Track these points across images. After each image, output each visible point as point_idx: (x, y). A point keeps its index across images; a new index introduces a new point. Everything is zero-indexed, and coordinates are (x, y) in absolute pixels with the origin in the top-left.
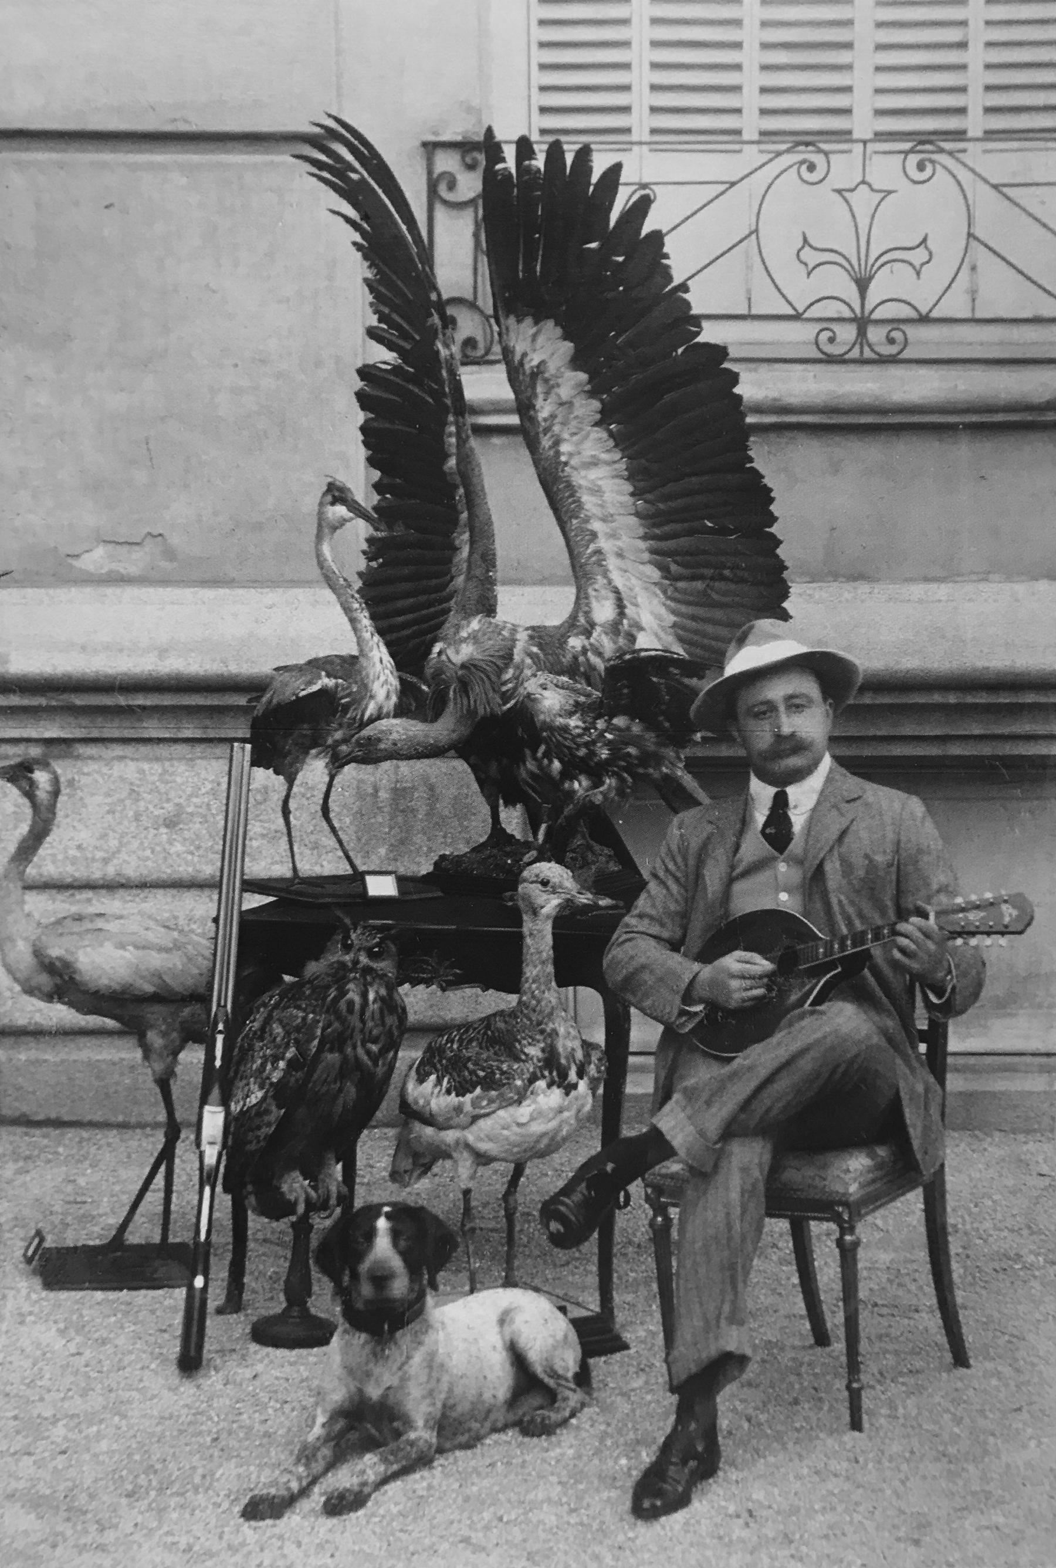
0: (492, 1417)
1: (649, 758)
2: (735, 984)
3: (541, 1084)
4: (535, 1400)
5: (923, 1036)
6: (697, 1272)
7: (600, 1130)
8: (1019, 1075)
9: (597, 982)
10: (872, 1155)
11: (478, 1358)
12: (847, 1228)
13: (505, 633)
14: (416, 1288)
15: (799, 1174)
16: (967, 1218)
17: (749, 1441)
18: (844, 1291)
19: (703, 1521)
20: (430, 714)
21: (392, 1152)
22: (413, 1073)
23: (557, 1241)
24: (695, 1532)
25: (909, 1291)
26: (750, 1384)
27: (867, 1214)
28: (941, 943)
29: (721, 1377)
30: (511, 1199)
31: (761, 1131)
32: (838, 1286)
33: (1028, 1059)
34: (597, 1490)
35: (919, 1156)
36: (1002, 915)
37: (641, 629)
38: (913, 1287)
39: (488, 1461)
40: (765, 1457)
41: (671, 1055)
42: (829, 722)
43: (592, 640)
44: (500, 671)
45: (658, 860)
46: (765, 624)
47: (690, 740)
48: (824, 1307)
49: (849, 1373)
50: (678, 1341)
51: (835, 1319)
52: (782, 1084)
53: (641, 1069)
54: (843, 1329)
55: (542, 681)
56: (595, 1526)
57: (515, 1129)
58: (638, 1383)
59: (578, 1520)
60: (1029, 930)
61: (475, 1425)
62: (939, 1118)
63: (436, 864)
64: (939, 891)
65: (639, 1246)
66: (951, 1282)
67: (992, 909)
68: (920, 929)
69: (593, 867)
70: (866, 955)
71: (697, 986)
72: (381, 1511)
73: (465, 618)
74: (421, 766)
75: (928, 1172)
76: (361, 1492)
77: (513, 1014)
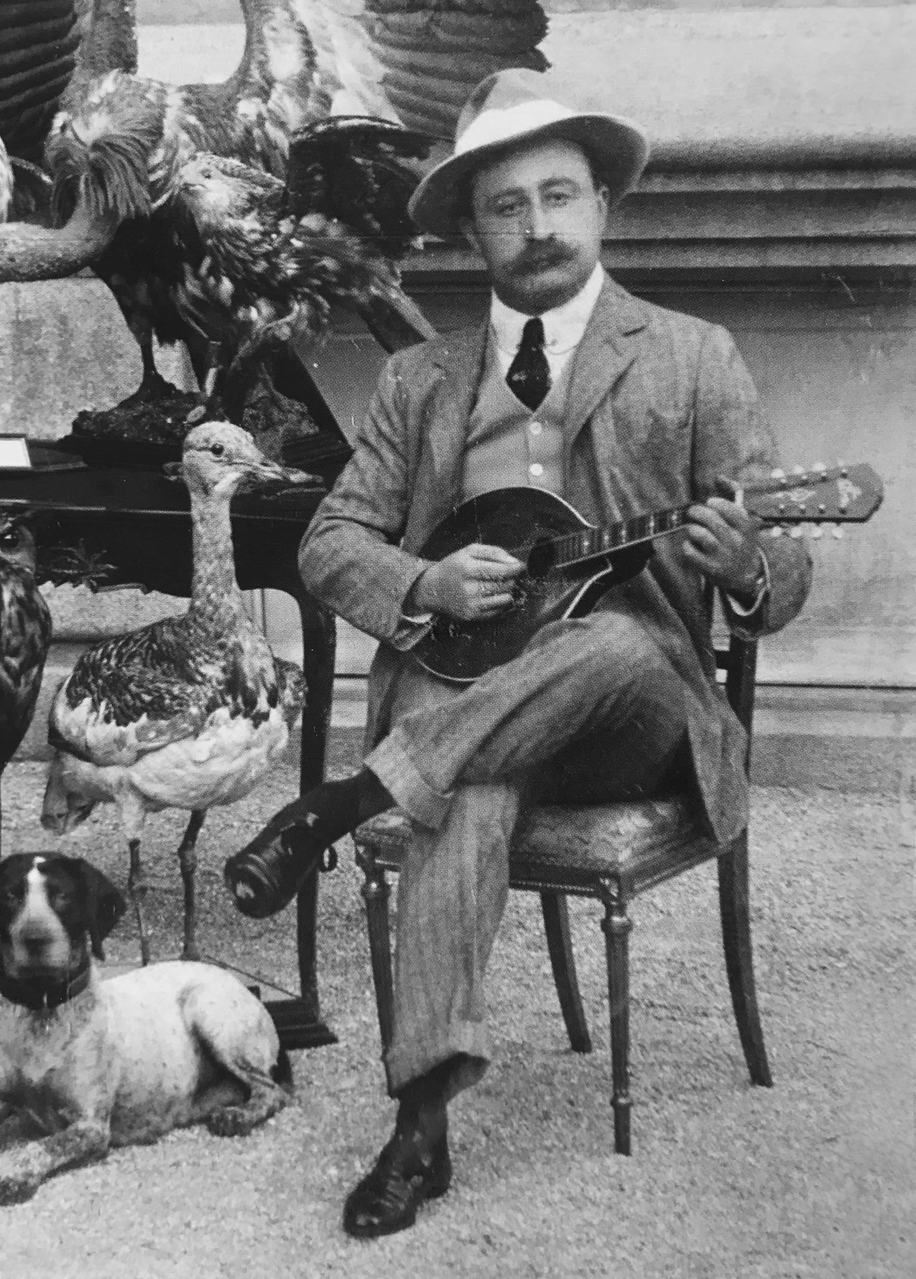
0: (174, 1110)
1: (353, 274)
2: (471, 587)
3: (222, 713)
4: (225, 1095)
5: (722, 660)
6: (421, 952)
7: (298, 773)
8: (857, 715)
9: (290, 581)
10: (649, 814)
11: (155, 1042)
12: (615, 906)
13: (151, 96)
14: (79, 956)
15: (551, 835)
16: (776, 900)
17: (487, 1158)
18: (610, 986)
19: (430, 1244)
20: (55, 215)
21: (42, 791)
22: (63, 695)
23: (246, 907)
24: (420, 1256)
25: (696, 990)
26: (488, 1092)
27: (642, 890)
28: (750, 535)
29: (452, 1081)
30: (188, 855)
31: (505, 777)
32: (603, 980)
33: (867, 694)
34: (301, 1201)
35: (713, 818)
36: (837, 496)
37: (339, 86)
38: (701, 985)
39: (172, 1160)
40: (506, 1178)
41: (389, 679)
42: (603, 221)
43: (270, 104)
44: (146, 152)
45: (368, 421)
46: (512, 77)
47: (409, 247)
48: (585, 1005)
49: (615, 1086)
50: (399, 1037)
51: (598, 1021)
52: (532, 719)
53: (350, 696)
54: (608, 1033)
55: (204, 166)
56: (300, 1240)
57: (193, 769)
58: (348, 1083)
59: (279, 1232)
60: (876, 516)
61: (155, 1119)
62: (741, 769)
63: (75, 425)
64: (751, 460)
65: (348, 918)
66: (751, 981)
67: (823, 486)
68: (722, 515)
69: (281, 429)
70: (647, 550)
71: (422, 591)
72: (50, 1206)
73: (94, 75)
74: (48, 289)
75: (724, 839)
76: (25, 1183)
77: (183, 623)
